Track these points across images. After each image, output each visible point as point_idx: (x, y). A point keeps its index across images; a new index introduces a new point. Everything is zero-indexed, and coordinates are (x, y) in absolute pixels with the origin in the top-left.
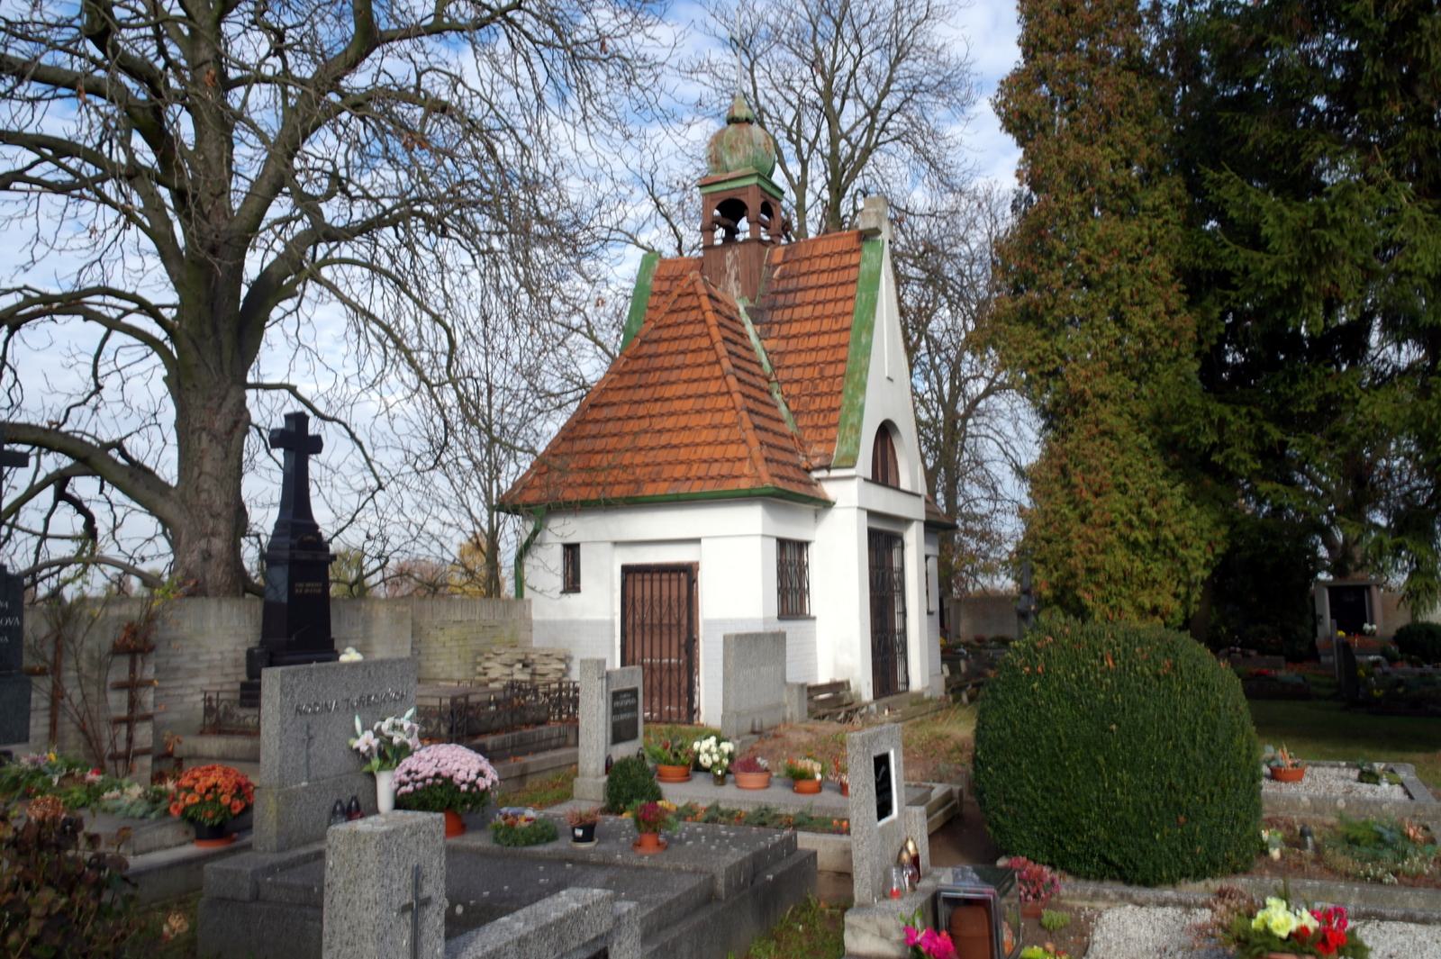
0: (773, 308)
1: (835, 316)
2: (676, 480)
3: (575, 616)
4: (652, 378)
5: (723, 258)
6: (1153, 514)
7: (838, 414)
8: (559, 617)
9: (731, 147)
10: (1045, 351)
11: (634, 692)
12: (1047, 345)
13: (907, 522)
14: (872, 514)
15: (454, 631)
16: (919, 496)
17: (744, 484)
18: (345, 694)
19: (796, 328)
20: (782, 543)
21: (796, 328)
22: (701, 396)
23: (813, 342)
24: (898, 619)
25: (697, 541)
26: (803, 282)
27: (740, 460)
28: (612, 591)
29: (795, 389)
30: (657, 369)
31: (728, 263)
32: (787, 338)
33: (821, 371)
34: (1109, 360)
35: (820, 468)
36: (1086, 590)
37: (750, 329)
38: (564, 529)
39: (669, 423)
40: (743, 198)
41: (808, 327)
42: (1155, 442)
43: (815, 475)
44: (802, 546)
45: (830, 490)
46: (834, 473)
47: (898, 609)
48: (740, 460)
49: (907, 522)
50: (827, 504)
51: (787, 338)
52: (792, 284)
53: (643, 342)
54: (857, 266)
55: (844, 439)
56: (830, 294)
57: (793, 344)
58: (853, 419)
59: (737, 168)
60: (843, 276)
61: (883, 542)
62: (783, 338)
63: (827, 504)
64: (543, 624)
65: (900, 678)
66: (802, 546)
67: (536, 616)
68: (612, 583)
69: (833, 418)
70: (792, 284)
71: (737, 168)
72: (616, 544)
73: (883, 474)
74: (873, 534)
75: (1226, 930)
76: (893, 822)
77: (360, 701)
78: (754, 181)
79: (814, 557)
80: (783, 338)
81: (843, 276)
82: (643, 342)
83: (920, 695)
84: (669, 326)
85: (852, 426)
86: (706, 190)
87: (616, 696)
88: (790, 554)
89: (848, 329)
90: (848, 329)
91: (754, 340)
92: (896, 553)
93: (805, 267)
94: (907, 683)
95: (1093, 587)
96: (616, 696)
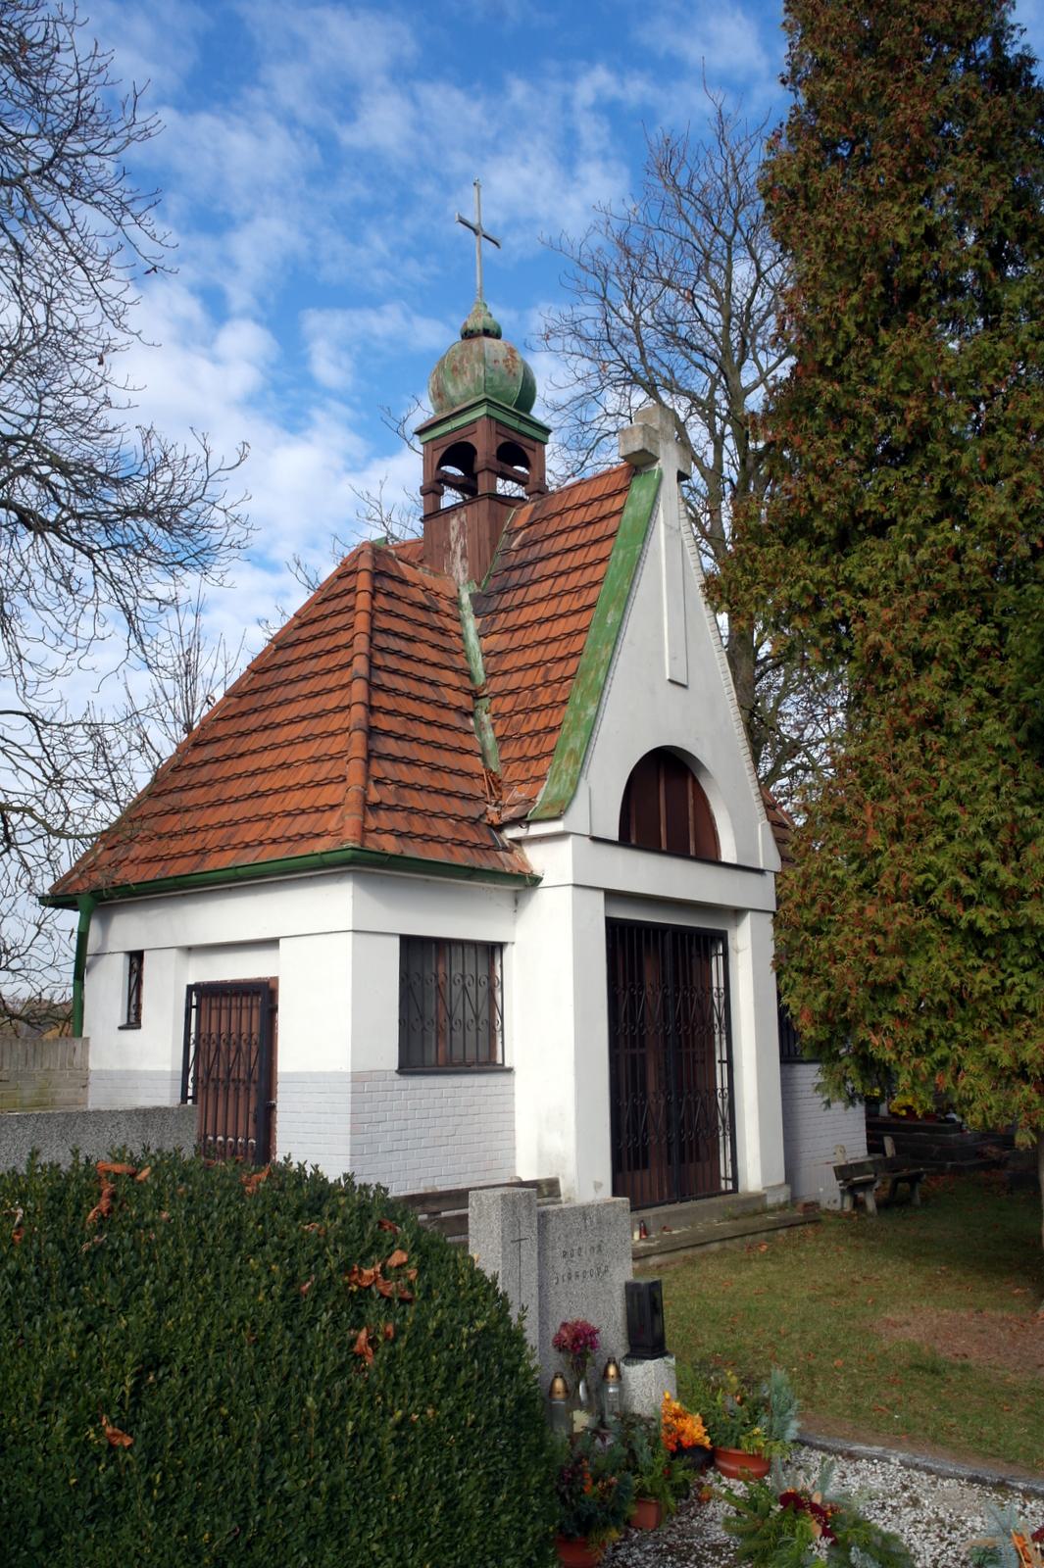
0: (502, 591)
1: (577, 590)
3: (134, 1065)
5: (446, 528)
6: (1006, 876)
7: (557, 735)
8: (117, 1067)
9: (455, 369)
10: (821, 583)
12: (823, 573)
13: (738, 913)
14: (612, 896)
16: (760, 872)
19: (528, 614)
21: (528, 614)
23: (542, 632)
24: (721, 1072)
25: (272, 943)
26: (548, 547)
29: (506, 705)
31: (453, 535)
34: (937, 587)
36: (875, 1027)
37: (471, 625)
38: (129, 929)
39: (266, 760)
40: (470, 440)
41: (543, 610)
42: (1022, 736)
43: (511, 833)
45: (537, 858)
46: (536, 830)
47: (720, 1054)
49: (738, 913)
50: (528, 882)
54: (619, 512)
55: (558, 773)
57: (519, 638)
59: (465, 398)
60: (600, 530)
62: (507, 630)
63: (528, 882)
64: (108, 1075)
65: (725, 1169)
67: (93, 1065)
69: (548, 742)
72: (190, 950)
74: (613, 927)
78: (482, 411)
80: (507, 630)
81: (600, 530)
83: (759, 1198)
86: (427, 437)
89: (591, 606)
90: (591, 606)
91: (472, 638)
92: (717, 964)
93: (554, 525)
94: (735, 1179)
95: (888, 1021)
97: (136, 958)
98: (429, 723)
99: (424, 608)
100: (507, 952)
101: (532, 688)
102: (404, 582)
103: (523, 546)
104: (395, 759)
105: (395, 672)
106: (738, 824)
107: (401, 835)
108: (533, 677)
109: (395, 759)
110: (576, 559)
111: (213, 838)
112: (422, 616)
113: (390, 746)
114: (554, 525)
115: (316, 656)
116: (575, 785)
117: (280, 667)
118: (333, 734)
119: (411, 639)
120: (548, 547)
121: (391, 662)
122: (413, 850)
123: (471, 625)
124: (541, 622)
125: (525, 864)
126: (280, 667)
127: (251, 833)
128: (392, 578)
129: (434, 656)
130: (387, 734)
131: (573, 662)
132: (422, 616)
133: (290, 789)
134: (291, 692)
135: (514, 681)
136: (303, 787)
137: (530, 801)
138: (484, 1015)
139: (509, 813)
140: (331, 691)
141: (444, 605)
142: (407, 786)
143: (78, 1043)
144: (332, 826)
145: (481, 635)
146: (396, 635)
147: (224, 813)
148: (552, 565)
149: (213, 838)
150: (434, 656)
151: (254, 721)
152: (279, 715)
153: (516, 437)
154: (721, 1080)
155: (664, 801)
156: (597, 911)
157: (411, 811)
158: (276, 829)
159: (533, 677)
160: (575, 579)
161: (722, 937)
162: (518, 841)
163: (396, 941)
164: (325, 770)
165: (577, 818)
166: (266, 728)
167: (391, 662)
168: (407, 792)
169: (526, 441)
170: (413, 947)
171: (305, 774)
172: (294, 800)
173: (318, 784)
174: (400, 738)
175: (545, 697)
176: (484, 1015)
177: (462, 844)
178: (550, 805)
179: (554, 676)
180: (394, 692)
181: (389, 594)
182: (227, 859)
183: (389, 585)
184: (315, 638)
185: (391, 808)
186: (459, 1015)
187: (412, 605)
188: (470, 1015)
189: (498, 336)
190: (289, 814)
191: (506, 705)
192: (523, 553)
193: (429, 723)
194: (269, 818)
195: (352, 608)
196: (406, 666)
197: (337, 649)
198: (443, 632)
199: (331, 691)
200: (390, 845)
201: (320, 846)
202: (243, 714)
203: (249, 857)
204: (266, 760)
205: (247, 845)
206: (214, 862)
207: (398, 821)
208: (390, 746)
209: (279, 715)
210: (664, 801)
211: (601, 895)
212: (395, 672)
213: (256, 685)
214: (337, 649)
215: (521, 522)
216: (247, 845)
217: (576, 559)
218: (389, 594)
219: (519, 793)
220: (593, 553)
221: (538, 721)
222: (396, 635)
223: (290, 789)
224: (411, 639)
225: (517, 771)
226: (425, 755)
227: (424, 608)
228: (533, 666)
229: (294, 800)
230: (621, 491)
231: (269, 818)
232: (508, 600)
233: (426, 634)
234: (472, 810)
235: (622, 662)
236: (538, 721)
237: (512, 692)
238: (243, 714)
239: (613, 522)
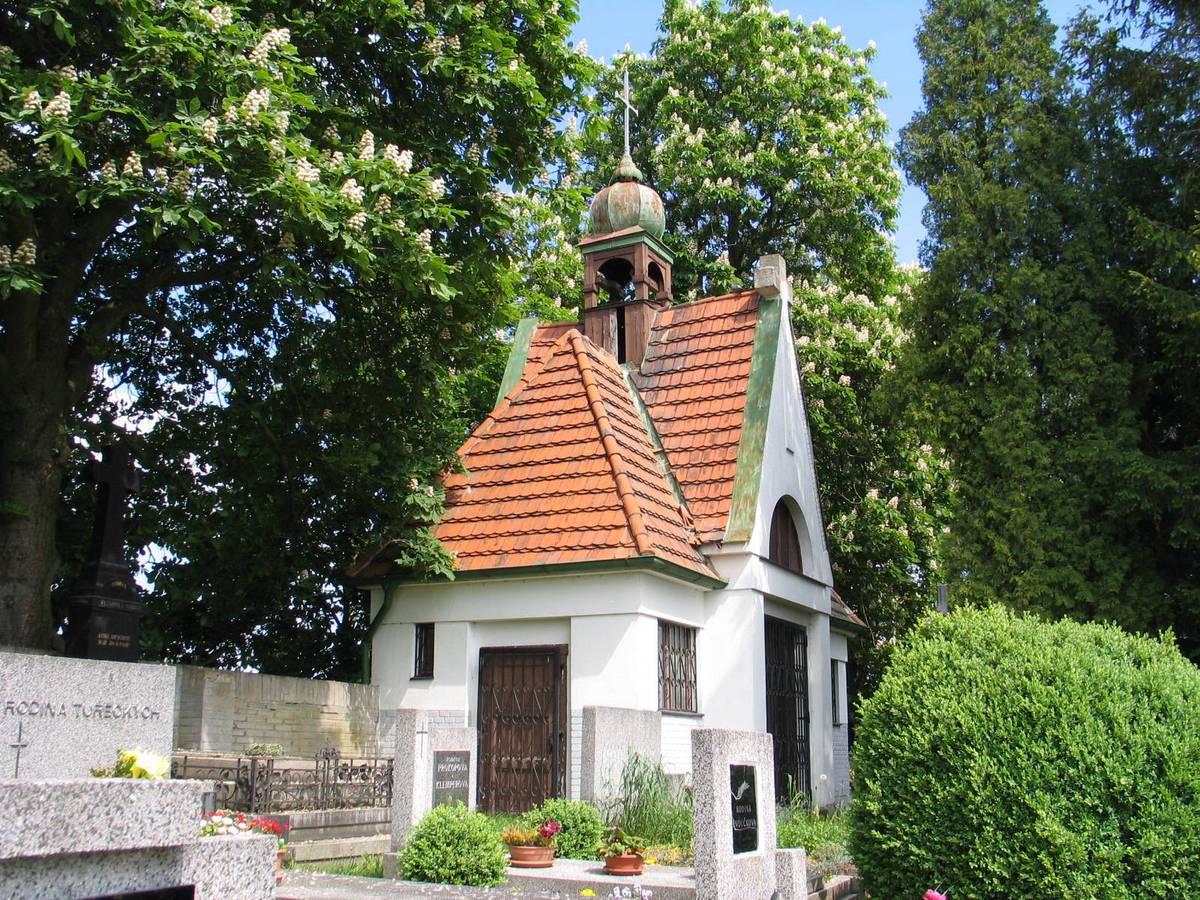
2: (544, 550)
11: (464, 757)
14: (769, 600)
15: (287, 713)
16: (824, 586)
17: (620, 554)
18: (77, 699)
20: (665, 626)
27: (617, 527)
28: (411, 892)
33: (713, 438)
44: (689, 633)
46: (725, 550)
48: (617, 527)
56: (724, 356)
61: (783, 636)
66: (689, 633)
68: (411, 892)
71: (623, 227)
73: (784, 552)
74: (771, 624)
75: (561, 37)
76: (758, 859)
77: (97, 710)
79: (703, 643)
82: (513, 404)
84: (543, 386)
85: (746, 497)
88: (675, 640)
92: (797, 652)
97: (426, 634)
178: (738, 533)
211: (761, 598)
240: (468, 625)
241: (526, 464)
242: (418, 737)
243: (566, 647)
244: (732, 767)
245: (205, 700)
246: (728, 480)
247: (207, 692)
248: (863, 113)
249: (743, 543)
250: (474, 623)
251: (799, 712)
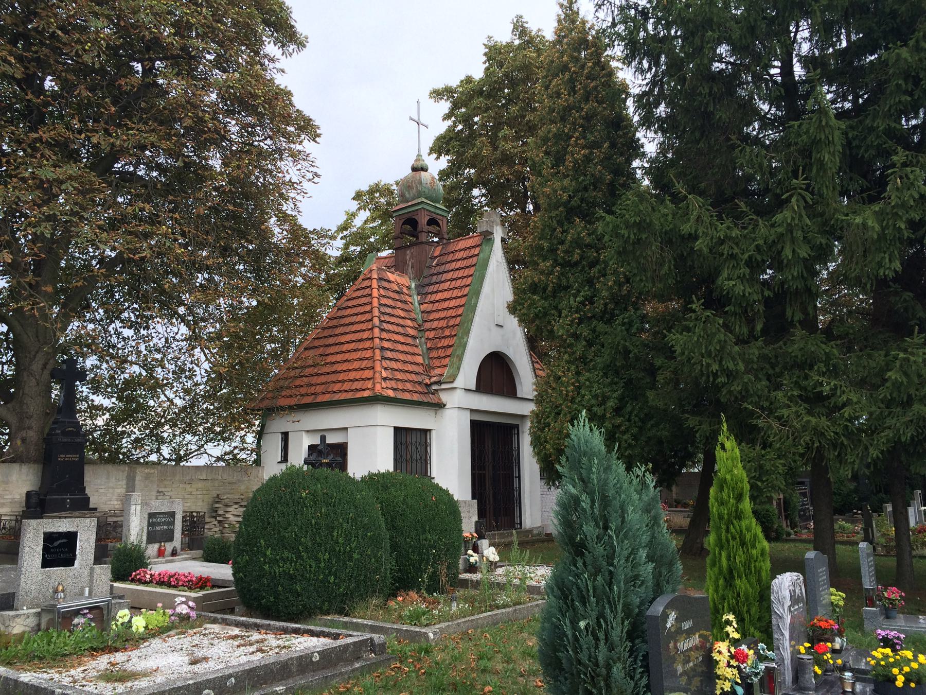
4: (338, 331)
5: (405, 254)
14: (472, 411)
15: (200, 485)
19: (439, 296)
21: (439, 296)
22: (359, 341)
23: (446, 305)
24: (516, 481)
25: (346, 429)
26: (448, 267)
29: (431, 334)
30: (341, 325)
32: (433, 302)
35: (435, 383)
39: (339, 358)
41: (446, 295)
43: (435, 387)
46: (443, 386)
49: (523, 417)
51: (433, 302)
52: (442, 268)
53: (339, 309)
57: (436, 306)
58: (459, 352)
62: (431, 302)
63: (440, 406)
70: (442, 268)
71: (413, 199)
74: (473, 423)
80: (431, 302)
82: (339, 309)
87: (151, 515)
92: (515, 438)
93: (450, 257)
96: (151, 515)
97: (285, 435)
98: (402, 343)
99: (397, 292)
100: (433, 434)
101: (442, 328)
102: (389, 281)
103: (437, 265)
104: (391, 359)
105: (388, 322)
106: (527, 379)
107: (394, 390)
108: (443, 323)
109: (391, 359)
110: (460, 273)
111: (319, 389)
112: (397, 296)
113: (389, 354)
114: (450, 257)
115: (356, 314)
116: (459, 369)
117: (340, 317)
118: (366, 349)
119: (393, 307)
120: (448, 267)
121: (387, 318)
122: (400, 395)
123: (416, 299)
124: (445, 300)
125: (440, 399)
126: (340, 317)
127: (337, 387)
128: (385, 280)
129: (402, 314)
130: (387, 349)
131: (459, 319)
132: (397, 296)
133: (350, 370)
134: (347, 329)
135: (435, 324)
136: (356, 370)
137: (442, 375)
138: (424, 457)
139: (433, 379)
140: (364, 330)
141: (405, 290)
142: (396, 370)
143: (260, 468)
144: (370, 386)
145: (420, 304)
146: (388, 306)
147: (323, 379)
148: (450, 275)
149: (319, 389)
150: (402, 314)
151: (331, 341)
152: (343, 339)
153: (434, 216)
154: (516, 485)
155: (496, 374)
156: (466, 419)
157: (398, 380)
158: (346, 386)
159: (443, 323)
160: (459, 283)
161: (517, 426)
162: (437, 390)
163: (391, 431)
164: (364, 364)
165: (460, 382)
166: (337, 344)
167: (387, 318)
168: (396, 373)
169: (439, 217)
170: (398, 431)
171: (356, 365)
172: (352, 375)
173: (362, 369)
174: (392, 350)
175: (447, 332)
176: (424, 457)
177: (416, 392)
178: (450, 377)
179: (451, 323)
180: (389, 331)
181: (384, 288)
182: (327, 398)
183: (385, 284)
184: (355, 306)
185: (391, 379)
186: (404, 457)
187: (393, 291)
188: (418, 457)
189: (426, 170)
190: (351, 381)
191: (431, 334)
192: (438, 268)
193: (402, 343)
194: (344, 381)
195: (371, 295)
196: (392, 320)
197: (365, 312)
198: (405, 302)
199: (364, 330)
200: (391, 393)
201: (366, 394)
202: (326, 337)
203: (337, 397)
204: (339, 358)
205: (335, 392)
206: (320, 399)
207: (393, 384)
208: (389, 354)
209: (343, 339)
210: (496, 374)
211: (468, 412)
212: (388, 322)
213: (330, 324)
214: (365, 312)
215: (437, 253)
216: (335, 392)
217: (460, 273)
218: (384, 288)
219: (438, 371)
220: (467, 272)
221: (445, 342)
222: (388, 306)
223: (350, 370)
224: (393, 307)
225: (437, 363)
226: (402, 357)
227: (397, 292)
228: (442, 319)
229: (352, 375)
230: (478, 246)
231: (344, 381)
232: (431, 289)
233: (399, 304)
234: (419, 379)
235: (477, 319)
236: (445, 342)
237: (434, 329)
238: (326, 337)
239: (475, 259)
240: (304, 433)
241: (337, 344)
242: (133, 507)
243: (346, 443)
244: (45, 534)
245: (137, 482)
246: (451, 346)
247: (138, 478)
248: (362, 211)
249: (452, 382)
250: (308, 431)
251: (516, 474)
